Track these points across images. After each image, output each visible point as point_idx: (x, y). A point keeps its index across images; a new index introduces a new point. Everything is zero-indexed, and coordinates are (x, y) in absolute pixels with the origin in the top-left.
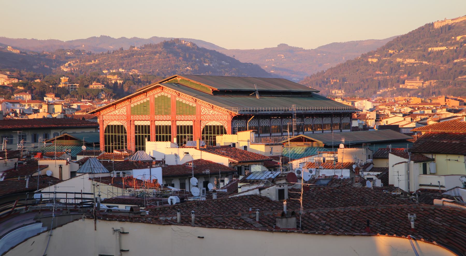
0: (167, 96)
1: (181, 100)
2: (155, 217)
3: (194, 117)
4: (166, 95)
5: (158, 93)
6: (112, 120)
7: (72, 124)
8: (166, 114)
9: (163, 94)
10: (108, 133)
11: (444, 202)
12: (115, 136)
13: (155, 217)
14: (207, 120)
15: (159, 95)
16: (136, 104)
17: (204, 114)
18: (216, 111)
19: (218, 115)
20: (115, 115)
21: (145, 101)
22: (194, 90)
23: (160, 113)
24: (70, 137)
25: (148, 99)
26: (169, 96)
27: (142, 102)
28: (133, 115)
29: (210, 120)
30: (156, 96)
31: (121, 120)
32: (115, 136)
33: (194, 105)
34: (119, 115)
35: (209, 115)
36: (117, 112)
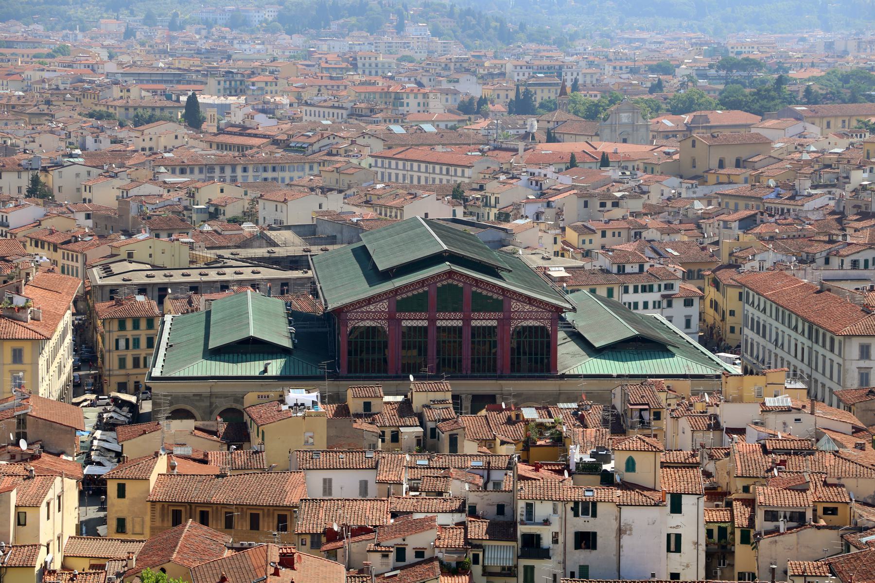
0: (457, 285)
1: (479, 291)
2: (118, 147)
3: (501, 315)
4: (455, 283)
5: (442, 280)
6: (362, 320)
7: (308, 66)
8: (455, 311)
9: (450, 281)
10: (369, 342)
11: (642, 412)
12: (536, 342)
13: (118, 147)
14: (520, 319)
15: (445, 283)
16: (404, 296)
17: (516, 311)
18: (534, 305)
19: (537, 312)
20: (368, 312)
21: (421, 291)
22: (63, 427)
23: (444, 309)
24: (501, 377)
25: (426, 289)
26: (461, 285)
27: (415, 292)
28: (400, 311)
29: (525, 319)
30: (439, 285)
31: (379, 319)
32: (536, 342)
33: (501, 298)
34: (376, 312)
35: (523, 311)
36: (372, 307)
